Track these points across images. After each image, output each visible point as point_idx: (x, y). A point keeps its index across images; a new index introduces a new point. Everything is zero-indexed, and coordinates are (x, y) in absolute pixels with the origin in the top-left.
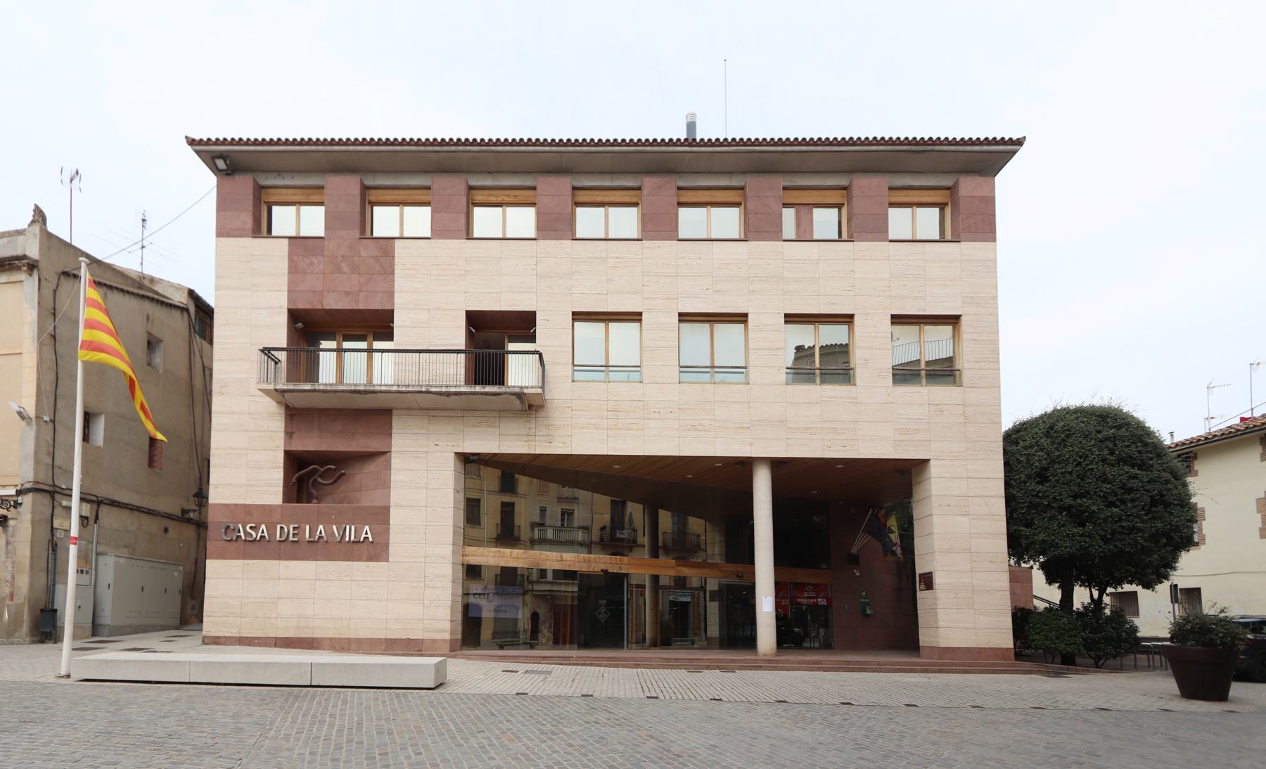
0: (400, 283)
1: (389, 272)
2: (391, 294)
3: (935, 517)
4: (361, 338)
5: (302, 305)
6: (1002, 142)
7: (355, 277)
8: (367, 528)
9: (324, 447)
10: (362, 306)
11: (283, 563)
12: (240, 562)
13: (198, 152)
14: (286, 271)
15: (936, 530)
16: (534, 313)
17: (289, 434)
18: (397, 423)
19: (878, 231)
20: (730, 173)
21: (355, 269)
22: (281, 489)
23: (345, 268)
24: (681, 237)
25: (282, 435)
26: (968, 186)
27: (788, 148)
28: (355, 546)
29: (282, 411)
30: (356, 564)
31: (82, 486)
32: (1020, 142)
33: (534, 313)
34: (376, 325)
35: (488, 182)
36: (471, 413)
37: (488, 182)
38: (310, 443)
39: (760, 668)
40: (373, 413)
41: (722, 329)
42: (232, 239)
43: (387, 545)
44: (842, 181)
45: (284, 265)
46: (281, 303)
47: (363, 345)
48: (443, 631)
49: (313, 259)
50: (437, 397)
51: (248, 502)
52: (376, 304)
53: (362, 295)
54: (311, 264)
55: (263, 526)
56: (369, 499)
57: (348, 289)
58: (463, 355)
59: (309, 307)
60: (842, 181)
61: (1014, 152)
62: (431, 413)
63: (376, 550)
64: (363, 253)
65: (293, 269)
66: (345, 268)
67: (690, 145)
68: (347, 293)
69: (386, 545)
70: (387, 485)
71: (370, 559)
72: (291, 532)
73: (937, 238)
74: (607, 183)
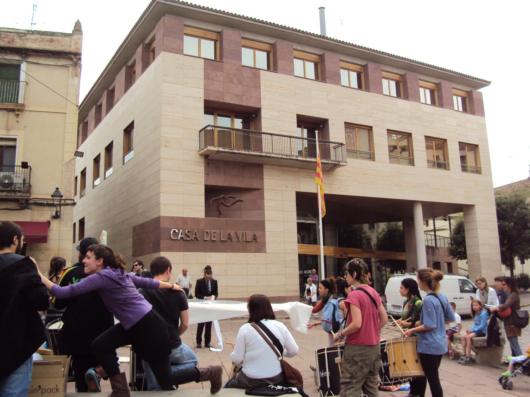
1: (258, 87)
2: (259, 99)
3: (478, 230)
5: (212, 98)
6: (484, 81)
7: (240, 87)
9: (227, 184)
11: (208, 254)
15: (479, 235)
17: (207, 174)
18: (267, 172)
21: (240, 83)
22: (204, 208)
23: (235, 81)
25: (203, 175)
28: (247, 243)
29: (202, 160)
30: (249, 254)
31: (324, 253)
32: (490, 82)
35: (299, 48)
36: (303, 170)
37: (299, 48)
38: (220, 181)
42: (171, 54)
43: (264, 243)
48: (296, 291)
49: (218, 73)
51: (185, 216)
52: (251, 104)
53: (244, 98)
54: (216, 75)
56: (251, 216)
57: (237, 93)
58: (436, 221)
59: (216, 100)
62: (283, 168)
64: (244, 75)
65: (207, 77)
66: (235, 80)
68: (237, 96)
70: (261, 208)
71: (256, 251)
74: (350, 60)
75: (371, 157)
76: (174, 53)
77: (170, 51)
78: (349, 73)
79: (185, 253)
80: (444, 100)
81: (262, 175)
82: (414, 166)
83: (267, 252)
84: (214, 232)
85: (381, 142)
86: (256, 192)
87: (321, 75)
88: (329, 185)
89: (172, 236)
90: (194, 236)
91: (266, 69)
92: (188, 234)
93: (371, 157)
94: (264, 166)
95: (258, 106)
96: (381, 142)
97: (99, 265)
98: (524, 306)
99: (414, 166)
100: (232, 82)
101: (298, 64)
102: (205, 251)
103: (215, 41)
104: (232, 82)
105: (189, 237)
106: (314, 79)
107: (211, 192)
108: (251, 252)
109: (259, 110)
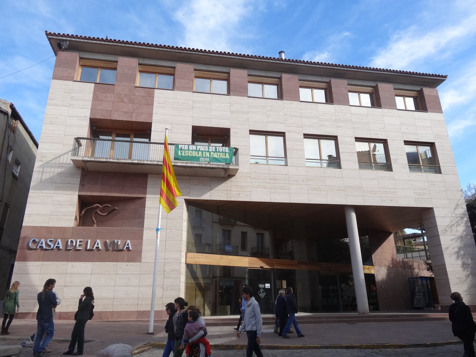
0: (156, 110)
2: (151, 115)
4: (128, 136)
5: (98, 117)
8: (98, 241)
10: (134, 120)
11: (70, 264)
12: (39, 263)
13: (49, 39)
14: (91, 99)
16: (230, 129)
17: (82, 186)
19: (243, 92)
20: (322, 76)
24: (249, 95)
26: (427, 91)
27: (123, 45)
29: (80, 172)
30: (119, 264)
32: (445, 77)
33: (230, 129)
34: (142, 131)
39: (322, 322)
40: (139, 176)
41: (271, 139)
44: (277, 75)
45: (91, 96)
46: (87, 114)
47: (110, 138)
49: (108, 95)
50: (99, 163)
52: (142, 119)
53: (134, 114)
55: (59, 240)
57: (126, 111)
59: (103, 118)
60: (277, 75)
61: (444, 80)
63: (134, 255)
64: (137, 94)
65: (96, 98)
66: (126, 100)
67: (279, 60)
68: (126, 113)
69: (140, 252)
71: (129, 261)
72: (78, 243)
73: (226, 93)
75: (388, 166)
76: (64, 80)
77: (59, 79)
78: (404, 99)
79: (43, 263)
80: (334, 96)
81: (146, 184)
82: (340, 168)
83: (142, 261)
84: (80, 241)
85: (399, 153)
86: (139, 201)
87: (376, 102)
88: (226, 192)
89: (30, 245)
90: (56, 245)
91: (325, 102)
92: (50, 243)
93: (388, 166)
94: (149, 175)
95: (148, 121)
96: (399, 153)
97: (469, 274)
98: (88, 341)
99: (340, 168)
100: (122, 101)
101: (399, 101)
102: (68, 260)
103: (325, 90)
104: (122, 101)
105: (50, 246)
106: (370, 106)
107: (84, 203)
108: (122, 261)
109: (150, 124)
